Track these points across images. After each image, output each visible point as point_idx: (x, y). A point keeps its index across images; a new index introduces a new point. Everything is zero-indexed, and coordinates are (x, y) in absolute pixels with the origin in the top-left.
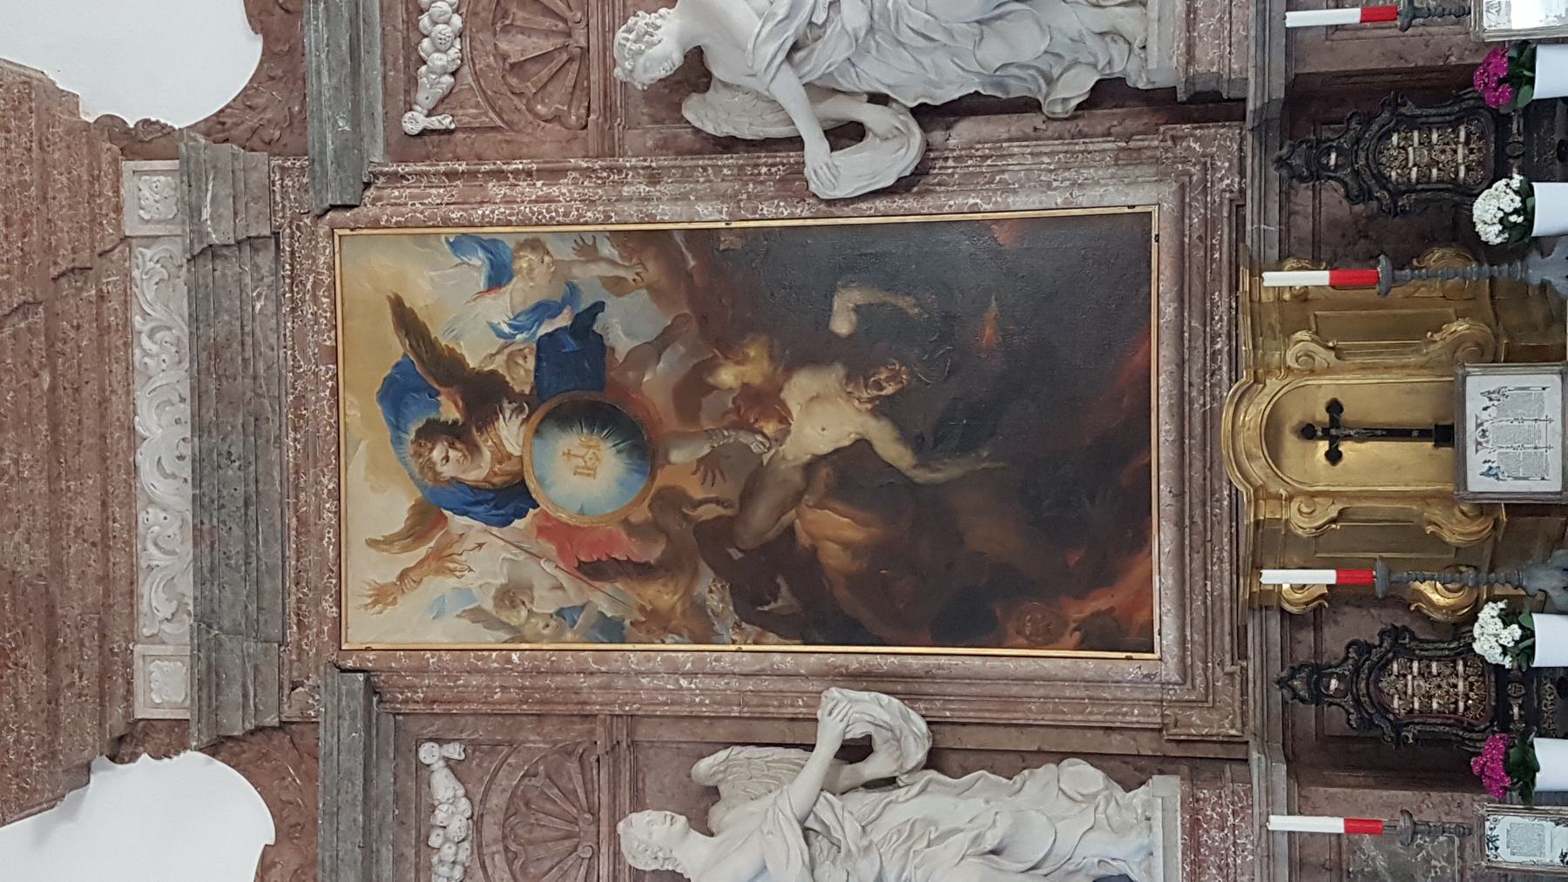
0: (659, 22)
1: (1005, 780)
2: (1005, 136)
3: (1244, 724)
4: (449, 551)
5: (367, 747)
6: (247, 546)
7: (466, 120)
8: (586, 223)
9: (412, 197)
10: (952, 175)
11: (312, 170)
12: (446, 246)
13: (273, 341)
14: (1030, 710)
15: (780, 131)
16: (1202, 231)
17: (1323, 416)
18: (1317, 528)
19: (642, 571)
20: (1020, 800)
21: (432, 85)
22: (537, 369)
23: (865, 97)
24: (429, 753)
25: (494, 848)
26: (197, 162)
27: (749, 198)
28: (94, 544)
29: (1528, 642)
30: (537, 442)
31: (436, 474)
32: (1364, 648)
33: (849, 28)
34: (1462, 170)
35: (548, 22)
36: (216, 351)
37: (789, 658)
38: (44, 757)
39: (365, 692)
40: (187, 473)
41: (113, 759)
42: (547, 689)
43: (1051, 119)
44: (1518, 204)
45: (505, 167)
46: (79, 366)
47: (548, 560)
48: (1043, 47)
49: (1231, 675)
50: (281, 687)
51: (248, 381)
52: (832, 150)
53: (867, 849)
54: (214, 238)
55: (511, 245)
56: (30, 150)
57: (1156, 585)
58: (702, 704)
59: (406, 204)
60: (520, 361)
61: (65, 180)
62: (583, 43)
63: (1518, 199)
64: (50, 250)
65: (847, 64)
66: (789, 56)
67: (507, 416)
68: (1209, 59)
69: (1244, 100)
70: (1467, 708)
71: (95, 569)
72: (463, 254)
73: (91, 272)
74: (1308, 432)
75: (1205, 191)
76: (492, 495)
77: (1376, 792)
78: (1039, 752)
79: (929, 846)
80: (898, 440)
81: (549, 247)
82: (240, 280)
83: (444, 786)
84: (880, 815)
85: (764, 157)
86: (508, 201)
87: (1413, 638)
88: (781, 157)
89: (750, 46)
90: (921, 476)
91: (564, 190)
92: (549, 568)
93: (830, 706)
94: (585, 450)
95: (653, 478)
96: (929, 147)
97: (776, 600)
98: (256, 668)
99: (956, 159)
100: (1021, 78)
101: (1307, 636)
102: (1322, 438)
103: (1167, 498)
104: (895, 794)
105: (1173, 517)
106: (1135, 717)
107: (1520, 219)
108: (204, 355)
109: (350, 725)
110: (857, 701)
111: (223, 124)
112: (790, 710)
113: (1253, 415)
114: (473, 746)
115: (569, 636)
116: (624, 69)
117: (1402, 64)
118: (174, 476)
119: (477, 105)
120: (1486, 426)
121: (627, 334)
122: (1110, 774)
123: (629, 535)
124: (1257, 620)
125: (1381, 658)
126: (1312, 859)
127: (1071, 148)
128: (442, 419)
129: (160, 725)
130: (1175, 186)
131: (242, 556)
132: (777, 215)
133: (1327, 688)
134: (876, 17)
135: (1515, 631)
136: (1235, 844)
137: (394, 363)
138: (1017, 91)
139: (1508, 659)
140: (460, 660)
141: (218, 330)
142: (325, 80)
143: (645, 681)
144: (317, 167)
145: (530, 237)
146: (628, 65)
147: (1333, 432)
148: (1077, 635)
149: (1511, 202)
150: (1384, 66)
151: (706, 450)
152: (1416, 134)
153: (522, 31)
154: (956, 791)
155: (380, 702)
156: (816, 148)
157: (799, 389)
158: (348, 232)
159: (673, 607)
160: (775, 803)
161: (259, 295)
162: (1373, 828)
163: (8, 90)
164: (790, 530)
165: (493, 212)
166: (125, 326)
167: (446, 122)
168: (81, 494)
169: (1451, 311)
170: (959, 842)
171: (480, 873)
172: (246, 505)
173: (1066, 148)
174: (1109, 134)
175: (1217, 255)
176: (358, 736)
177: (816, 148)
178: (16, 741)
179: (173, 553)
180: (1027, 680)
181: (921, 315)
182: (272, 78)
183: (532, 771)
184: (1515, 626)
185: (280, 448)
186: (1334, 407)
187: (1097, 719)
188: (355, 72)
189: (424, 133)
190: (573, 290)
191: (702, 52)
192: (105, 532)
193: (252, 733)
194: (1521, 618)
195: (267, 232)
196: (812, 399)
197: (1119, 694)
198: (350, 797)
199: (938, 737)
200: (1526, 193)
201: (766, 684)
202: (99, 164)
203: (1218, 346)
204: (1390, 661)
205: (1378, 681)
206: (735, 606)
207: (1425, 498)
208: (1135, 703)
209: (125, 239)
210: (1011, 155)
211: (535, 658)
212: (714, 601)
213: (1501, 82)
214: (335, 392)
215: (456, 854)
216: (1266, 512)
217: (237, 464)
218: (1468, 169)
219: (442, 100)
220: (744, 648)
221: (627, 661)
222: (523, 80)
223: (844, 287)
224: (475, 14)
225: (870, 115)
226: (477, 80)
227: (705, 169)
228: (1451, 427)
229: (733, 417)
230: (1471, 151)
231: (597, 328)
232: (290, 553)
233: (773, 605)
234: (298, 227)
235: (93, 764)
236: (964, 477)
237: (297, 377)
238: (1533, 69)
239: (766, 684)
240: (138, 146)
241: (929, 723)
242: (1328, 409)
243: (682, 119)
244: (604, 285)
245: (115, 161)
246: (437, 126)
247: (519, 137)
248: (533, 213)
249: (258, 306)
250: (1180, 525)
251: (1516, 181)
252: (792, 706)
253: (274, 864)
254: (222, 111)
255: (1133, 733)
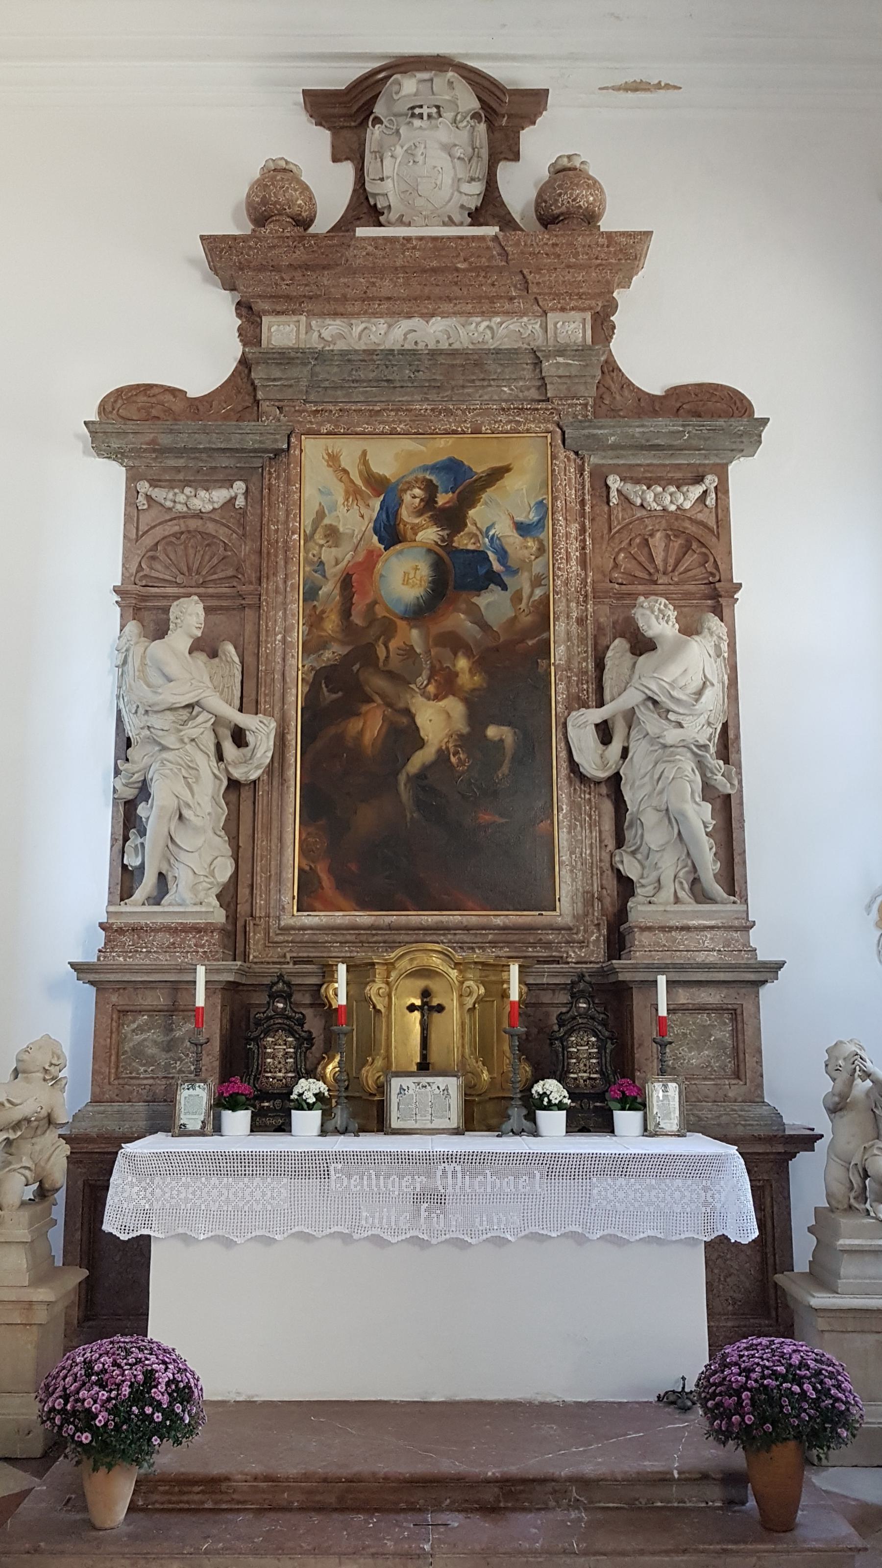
0: (670, 623)
1: (222, 825)
2: (602, 829)
3: (256, 963)
4: (358, 497)
5: (243, 450)
6: (363, 381)
7: (615, 512)
8: (554, 580)
9: (570, 479)
10: (580, 797)
11: (585, 421)
12: (541, 498)
13: (486, 397)
14: (262, 841)
15: (607, 696)
16: (544, 940)
17: (435, 1002)
18: (370, 998)
19: (346, 612)
20: (210, 833)
21: (635, 492)
22: (468, 551)
23: (626, 745)
24: (239, 487)
25: (183, 525)
26: (591, 355)
27: (568, 677)
28: (365, 292)
29: (305, 1106)
30: (424, 550)
31: (405, 491)
32: (301, 1022)
33: (665, 733)
34: (575, 1076)
35: (671, 561)
36: (478, 364)
37: (294, 698)
38: (240, 263)
39: (276, 450)
40: (407, 347)
41: (239, 304)
42: (276, 556)
43: (612, 855)
44: (554, 1102)
45: (587, 534)
46: (471, 285)
47: (353, 557)
48: (653, 847)
49: (285, 956)
50: (280, 400)
51: (461, 382)
52: (597, 725)
53: (182, 741)
54: (545, 364)
55: (541, 536)
56: (597, 258)
57: (337, 914)
58: (266, 648)
59: (565, 475)
60: (473, 541)
61: (580, 278)
62: (660, 582)
63: (557, 1102)
64: (539, 270)
65: (645, 733)
66: (650, 698)
67: (440, 533)
68: (642, 939)
69: (620, 959)
70: (268, 1078)
71: (350, 293)
72: (536, 508)
73: (525, 293)
74: (426, 994)
75: (568, 942)
76: (392, 523)
77: (218, 1031)
78: (238, 847)
79: (184, 777)
80: (424, 764)
81: (540, 558)
82: (521, 379)
83: (220, 495)
84: (201, 750)
85: (592, 687)
86: (567, 535)
87: (307, 1049)
88: (593, 696)
89: (655, 675)
90: (402, 778)
91: (573, 568)
92: (348, 557)
93: (265, 721)
94: (419, 578)
95: (402, 618)
96: (598, 783)
97: (328, 691)
98: (291, 386)
99: (590, 799)
100: (635, 836)
101: (307, 1000)
102: (422, 1001)
103: (388, 920)
104: (213, 759)
105: (377, 923)
106: (260, 902)
107: (545, 1103)
108: (476, 357)
109: (256, 440)
110: (268, 738)
111: (613, 371)
112: (263, 700)
113: (436, 961)
114: (243, 512)
115: (308, 569)
116: (643, 602)
117: (636, 1046)
118: (405, 339)
119: (624, 519)
120: (428, 1087)
121: (488, 604)
122: (225, 887)
123: (368, 605)
124: (316, 970)
125: (296, 1032)
126: (179, 995)
127: (595, 866)
128: (438, 495)
129: (258, 330)
130: (571, 924)
131: (358, 378)
132: (558, 693)
133: (278, 1002)
134: (671, 749)
135: (312, 1100)
136: (188, 952)
137: (472, 466)
138: (629, 835)
139: (296, 1097)
140: (294, 505)
141: (492, 366)
142: (638, 430)
143: (280, 613)
144: (587, 424)
145: (546, 548)
146: (645, 604)
147: (426, 1007)
148: (307, 868)
149: (555, 1098)
150: (635, 1035)
151: (418, 651)
152: (596, 1050)
153: (667, 546)
154: (215, 797)
155: (270, 458)
156: (596, 715)
157: (454, 706)
158: (549, 441)
159: (325, 630)
160: (208, 688)
161: (512, 390)
162: (198, 1024)
163: (632, 247)
164: (369, 700)
165: (561, 526)
166: (493, 312)
167: (614, 501)
168: (395, 286)
169: (495, 1075)
170: (186, 795)
171: (168, 518)
172: (388, 381)
173: (595, 862)
174: (602, 888)
175: (530, 949)
176: (250, 445)
177: (596, 715)
178: (250, 247)
179: (360, 339)
180: (281, 839)
181: (498, 777)
182: (639, 400)
183: (228, 548)
184: (314, 1100)
185: (422, 400)
186: (440, 1008)
187: (258, 879)
188: (642, 448)
189: (608, 488)
190: (515, 572)
191: (654, 649)
192: (373, 299)
193: (253, 384)
194: (319, 1103)
195: (549, 395)
196: (448, 714)
197: (272, 892)
198: (214, 439)
199: (247, 788)
200: (560, 1106)
201: (278, 685)
202: (589, 299)
203: (477, 951)
204: (294, 1036)
205: (283, 1029)
206: (325, 667)
207: (388, 1057)
208: (268, 902)
209: (545, 313)
210: (591, 832)
211: (295, 549)
212: (327, 655)
213: (623, 1092)
214: (455, 432)
215: (180, 503)
216: (380, 970)
217: (412, 376)
218: (575, 1079)
219: (627, 498)
220: (300, 672)
221: (292, 602)
222: (638, 545)
223: (515, 732)
224: (677, 519)
225: (616, 747)
226: (638, 519)
227: (586, 652)
228: (428, 1069)
229: (438, 667)
230: (585, 1081)
231: (492, 586)
232: (359, 407)
233: (325, 689)
234: (552, 413)
235: (236, 292)
236: (401, 802)
237: (464, 411)
238: (629, 1109)
239: (278, 685)
240: (599, 322)
241: (254, 782)
242: (439, 1005)
243: (615, 638)
244: (517, 591)
245: (591, 308)
246: (612, 495)
247: (605, 542)
248: (560, 549)
249: (505, 389)
250: (371, 927)
251: (567, 1101)
252: (265, 701)
253: (175, 397)
254: (620, 370)
255: (250, 901)
